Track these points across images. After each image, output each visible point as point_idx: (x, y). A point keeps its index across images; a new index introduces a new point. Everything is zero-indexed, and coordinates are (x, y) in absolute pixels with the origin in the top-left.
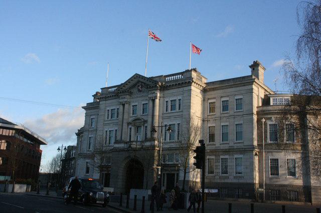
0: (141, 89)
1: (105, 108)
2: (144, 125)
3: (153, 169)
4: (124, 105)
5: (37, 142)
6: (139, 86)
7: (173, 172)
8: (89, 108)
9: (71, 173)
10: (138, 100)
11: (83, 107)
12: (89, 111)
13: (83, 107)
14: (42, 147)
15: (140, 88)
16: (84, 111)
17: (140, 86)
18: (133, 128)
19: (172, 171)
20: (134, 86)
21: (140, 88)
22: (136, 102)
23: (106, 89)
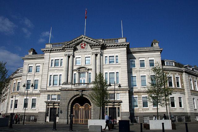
0: (84, 46)
6: (82, 44)
21: (83, 46)
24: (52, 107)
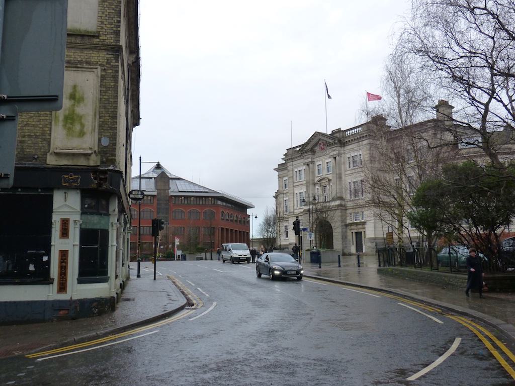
0: (323, 147)
1: (293, 170)
2: (329, 185)
3: (424, 229)
4: (335, 158)
5: (242, 208)
6: (320, 144)
7: (360, 231)
8: (281, 168)
9: (423, 246)
10: (324, 161)
11: (275, 169)
12: (281, 173)
13: (275, 169)
14: (249, 211)
15: (321, 146)
16: (277, 173)
17: (322, 144)
18: (319, 188)
19: (360, 228)
20: (316, 144)
22: (319, 161)
23: (291, 150)
24: (356, 231)
